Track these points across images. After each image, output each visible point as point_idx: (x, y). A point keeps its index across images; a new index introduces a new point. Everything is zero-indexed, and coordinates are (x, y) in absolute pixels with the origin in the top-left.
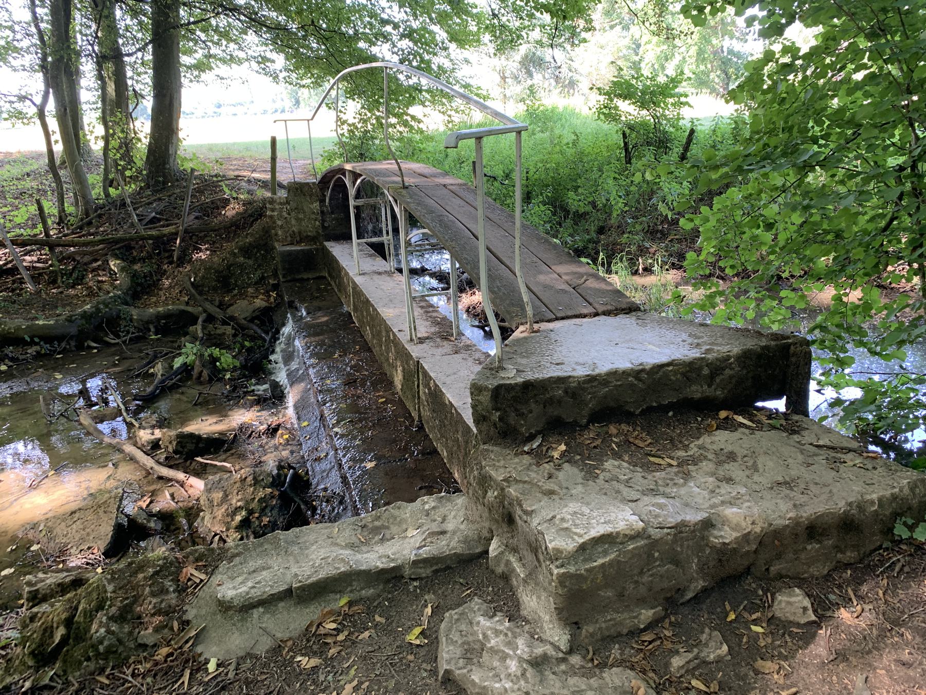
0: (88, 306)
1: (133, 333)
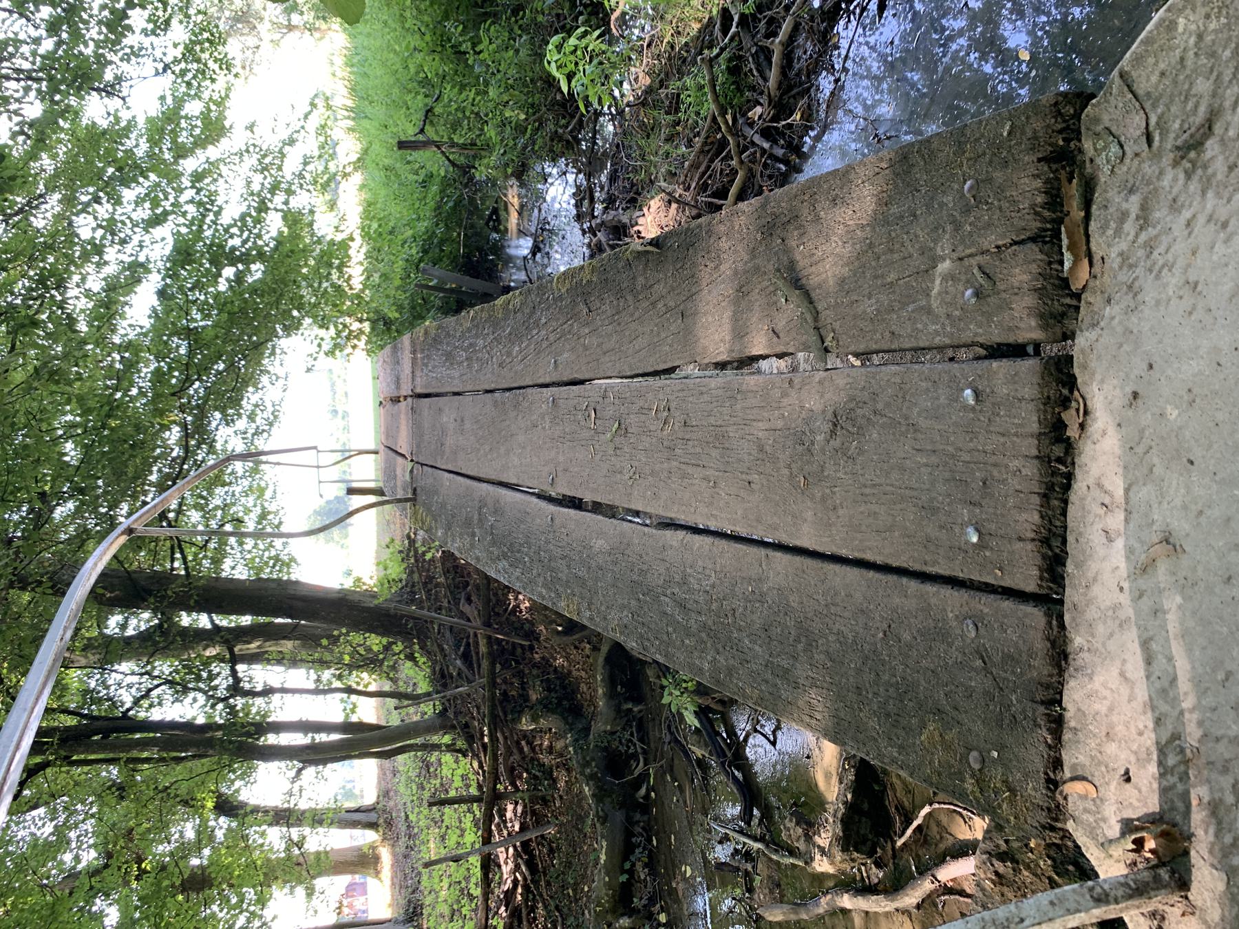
0: (587, 789)
1: (632, 734)
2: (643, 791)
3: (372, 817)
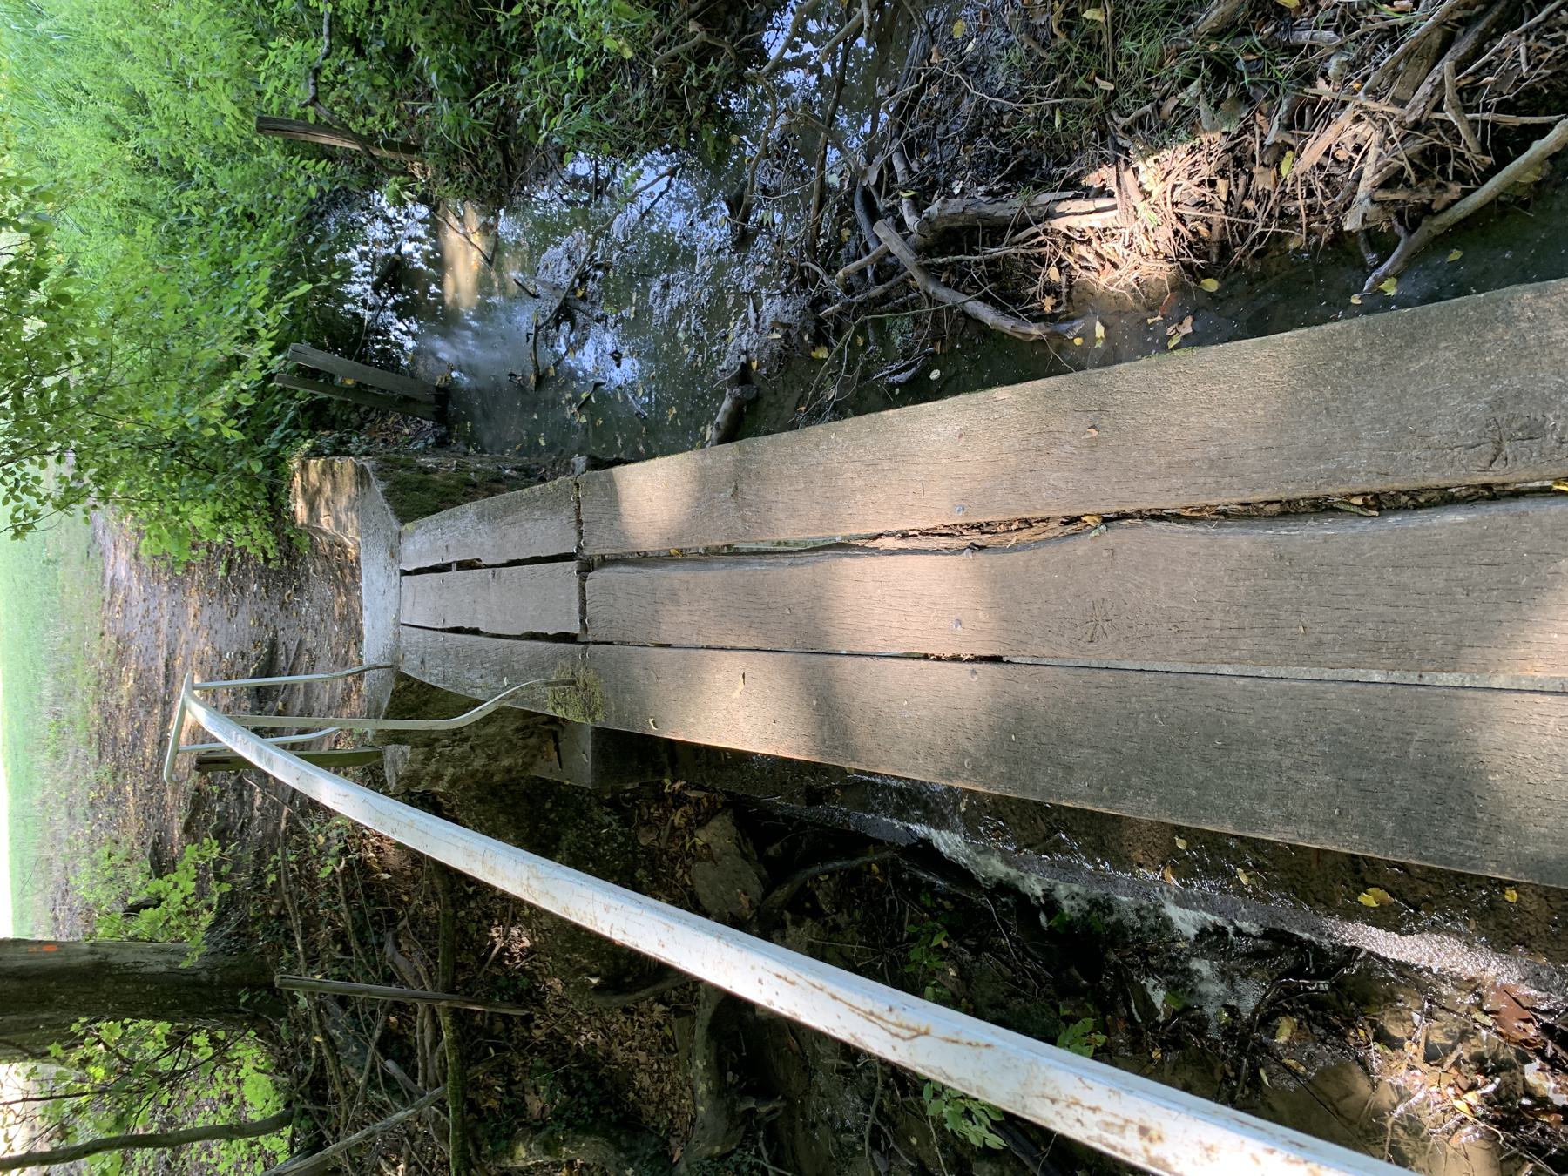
1: (758, 1155)
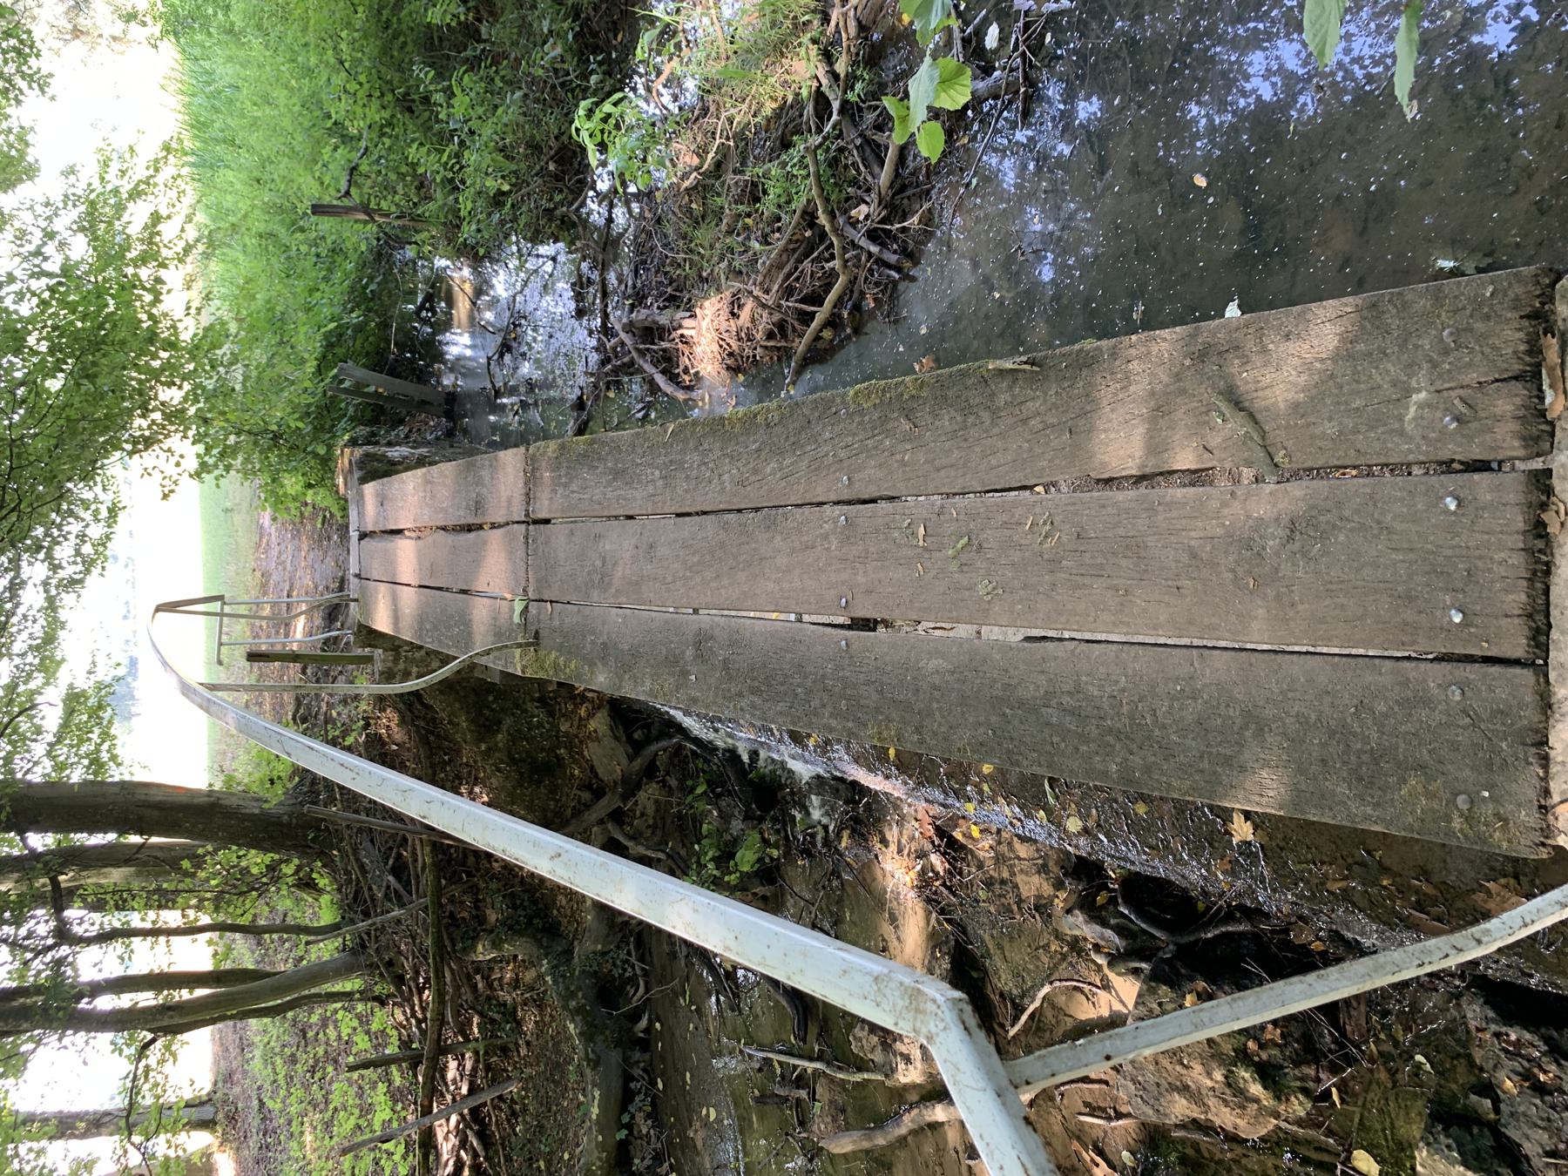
0: (572, 1027)
1: (629, 953)
2: (644, 1023)
3: (207, 1113)
